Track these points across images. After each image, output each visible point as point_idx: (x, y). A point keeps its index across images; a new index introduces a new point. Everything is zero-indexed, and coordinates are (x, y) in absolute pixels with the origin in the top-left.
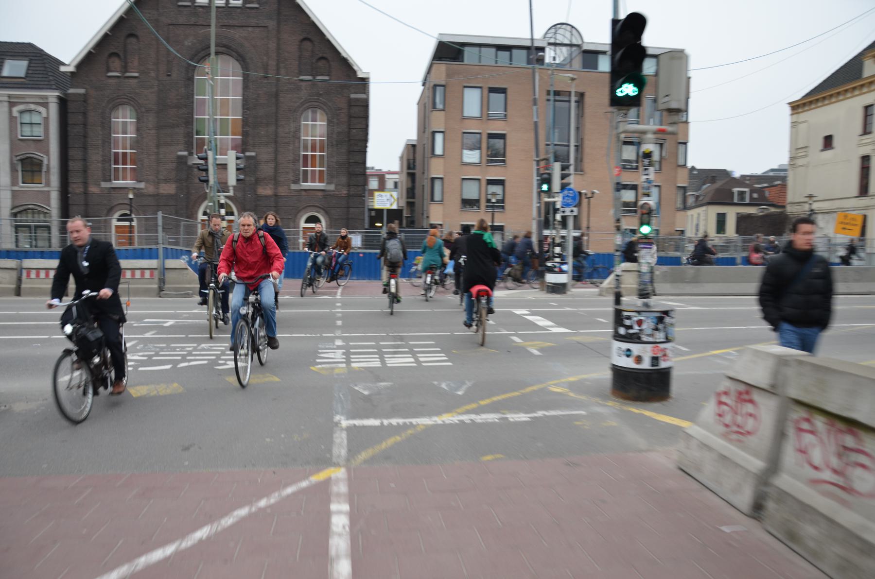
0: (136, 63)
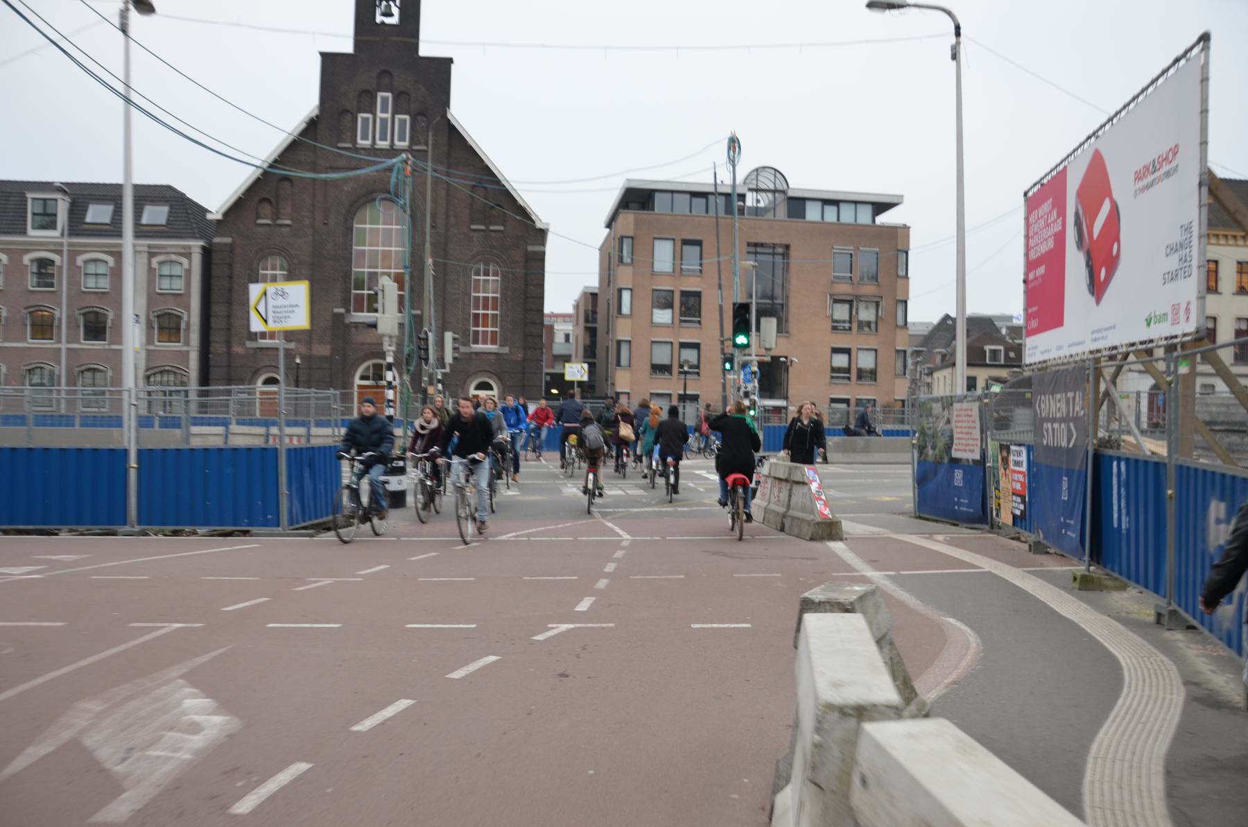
0: (289, 209)
